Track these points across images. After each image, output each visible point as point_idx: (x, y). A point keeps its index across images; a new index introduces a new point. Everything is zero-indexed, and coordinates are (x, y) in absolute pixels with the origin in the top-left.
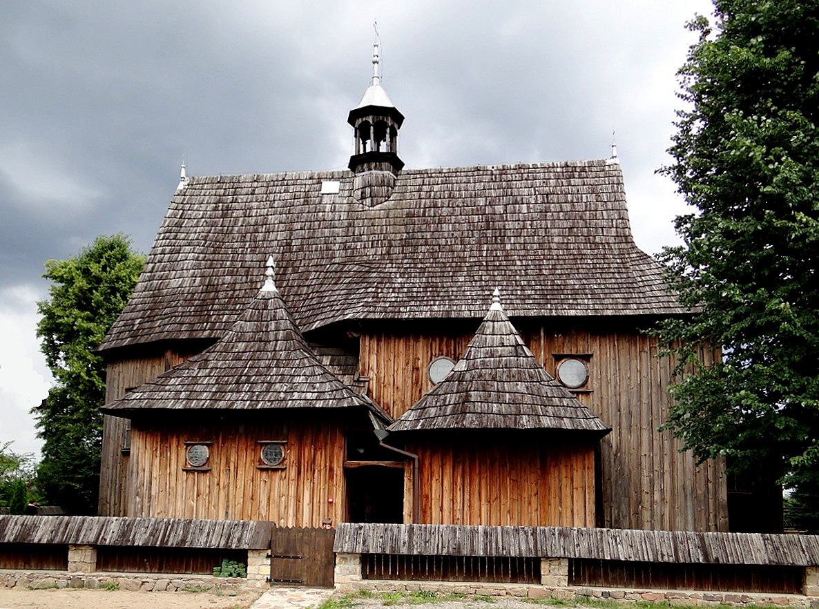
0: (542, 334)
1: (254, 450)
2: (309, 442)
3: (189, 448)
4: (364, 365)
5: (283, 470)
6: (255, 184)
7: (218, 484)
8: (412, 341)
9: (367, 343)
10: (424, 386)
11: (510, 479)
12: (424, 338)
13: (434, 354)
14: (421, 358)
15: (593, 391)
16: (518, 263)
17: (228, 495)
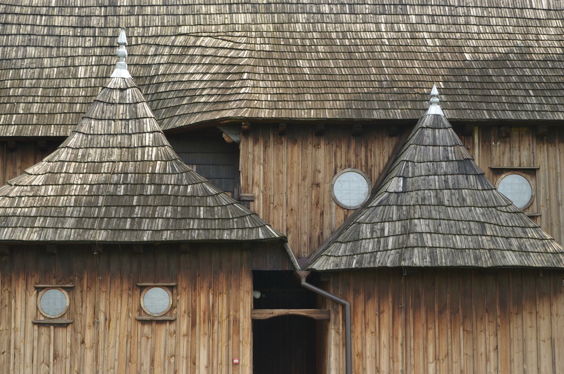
2: (205, 285)
3: (41, 293)
4: (247, 179)
5: (171, 322)
7: (83, 342)
8: (310, 147)
10: (327, 210)
11: (464, 330)
12: (325, 144)
13: (339, 165)
14: (322, 171)
15: (540, 216)
16: (429, 42)
17: (96, 357)
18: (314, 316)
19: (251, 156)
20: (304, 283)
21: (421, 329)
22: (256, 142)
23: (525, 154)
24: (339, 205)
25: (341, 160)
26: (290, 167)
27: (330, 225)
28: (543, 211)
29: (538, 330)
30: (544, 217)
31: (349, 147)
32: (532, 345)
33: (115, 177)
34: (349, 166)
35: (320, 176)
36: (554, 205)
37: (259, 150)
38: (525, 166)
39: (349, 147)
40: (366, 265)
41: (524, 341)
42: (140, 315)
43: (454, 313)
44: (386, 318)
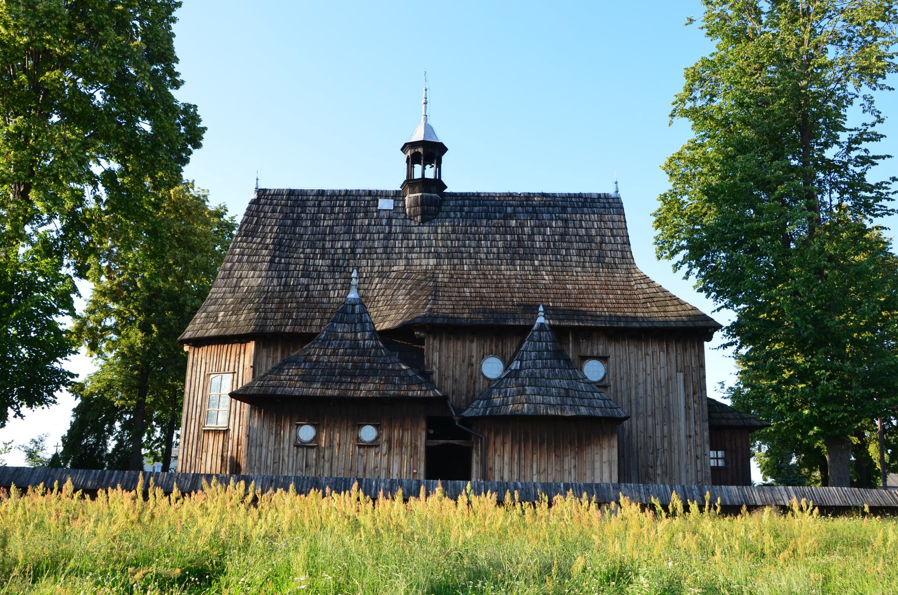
0: (571, 339)
1: (353, 430)
4: (428, 360)
5: (376, 446)
6: (320, 198)
7: (323, 457)
8: (468, 342)
9: (431, 342)
18: (463, 444)
19: (431, 347)
20: (457, 424)
21: (529, 455)
22: (434, 338)
23: (601, 347)
24: (485, 377)
25: (487, 350)
26: (455, 354)
27: (479, 389)
28: (612, 383)
29: (601, 456)
30: (612, 387)
31: (492, 342)
32: (597, 465)
33: (346, 358)
34: (492, 354)
35: (474, 360)
36: (618, 379)
37: (436, 344)
38: (601, 354)
39: (492, 342)
40: (494, 413)
41: (593, 462)
42: (358, 442)
43: (549, 445)
44: (508, 447)
